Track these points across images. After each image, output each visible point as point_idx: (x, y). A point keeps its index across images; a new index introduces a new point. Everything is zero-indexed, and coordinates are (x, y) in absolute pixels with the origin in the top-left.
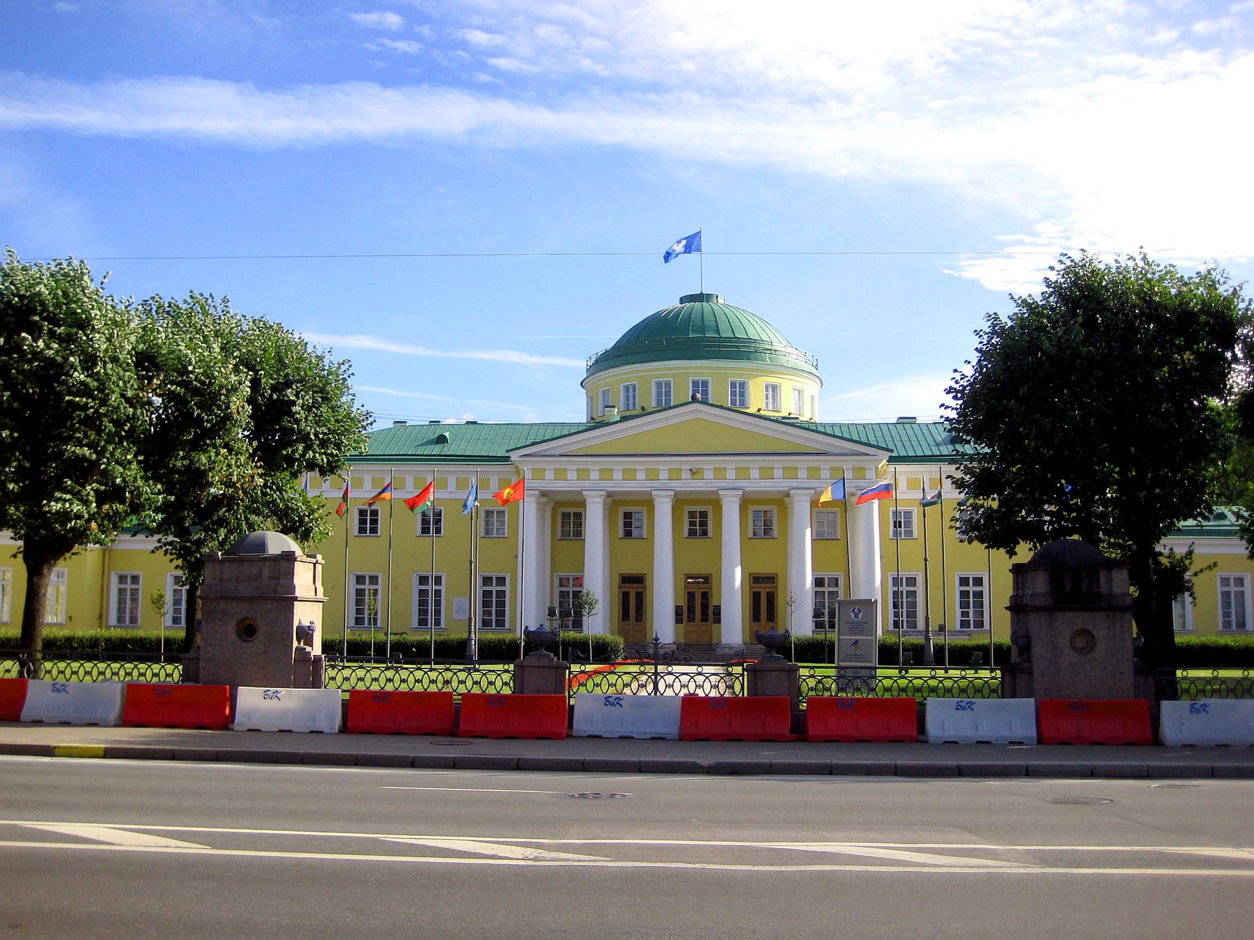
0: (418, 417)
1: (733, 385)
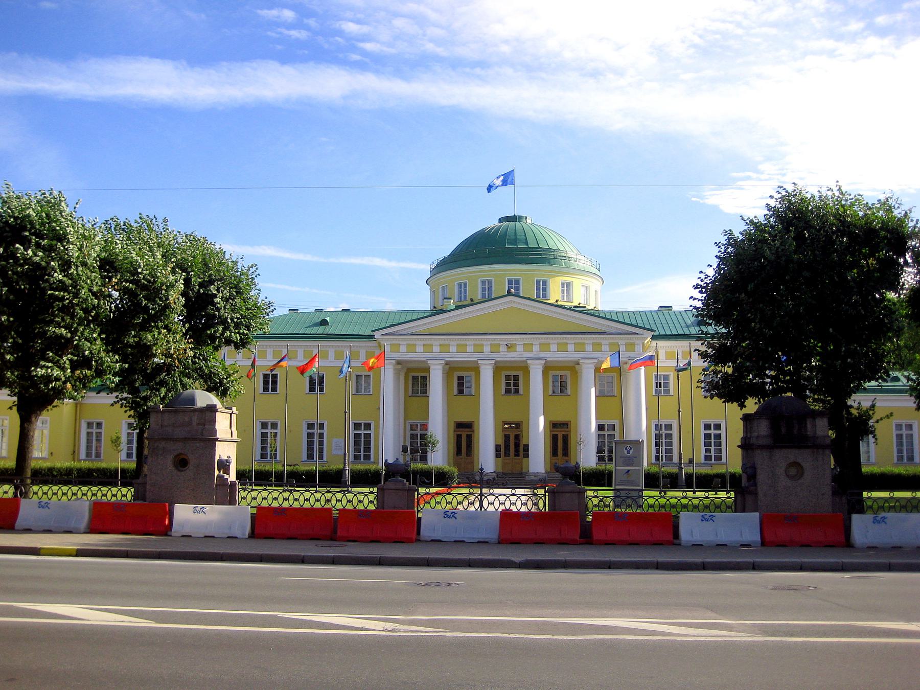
0: (306, 306)
1: (538, 282)
